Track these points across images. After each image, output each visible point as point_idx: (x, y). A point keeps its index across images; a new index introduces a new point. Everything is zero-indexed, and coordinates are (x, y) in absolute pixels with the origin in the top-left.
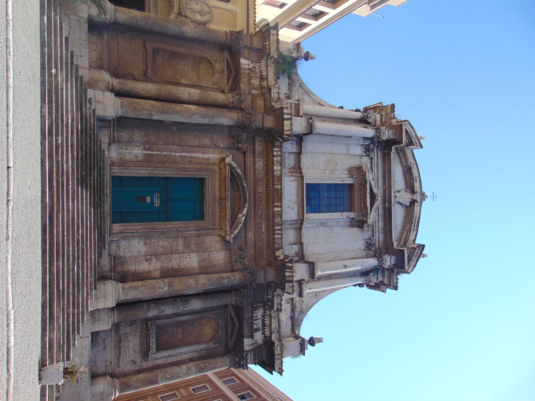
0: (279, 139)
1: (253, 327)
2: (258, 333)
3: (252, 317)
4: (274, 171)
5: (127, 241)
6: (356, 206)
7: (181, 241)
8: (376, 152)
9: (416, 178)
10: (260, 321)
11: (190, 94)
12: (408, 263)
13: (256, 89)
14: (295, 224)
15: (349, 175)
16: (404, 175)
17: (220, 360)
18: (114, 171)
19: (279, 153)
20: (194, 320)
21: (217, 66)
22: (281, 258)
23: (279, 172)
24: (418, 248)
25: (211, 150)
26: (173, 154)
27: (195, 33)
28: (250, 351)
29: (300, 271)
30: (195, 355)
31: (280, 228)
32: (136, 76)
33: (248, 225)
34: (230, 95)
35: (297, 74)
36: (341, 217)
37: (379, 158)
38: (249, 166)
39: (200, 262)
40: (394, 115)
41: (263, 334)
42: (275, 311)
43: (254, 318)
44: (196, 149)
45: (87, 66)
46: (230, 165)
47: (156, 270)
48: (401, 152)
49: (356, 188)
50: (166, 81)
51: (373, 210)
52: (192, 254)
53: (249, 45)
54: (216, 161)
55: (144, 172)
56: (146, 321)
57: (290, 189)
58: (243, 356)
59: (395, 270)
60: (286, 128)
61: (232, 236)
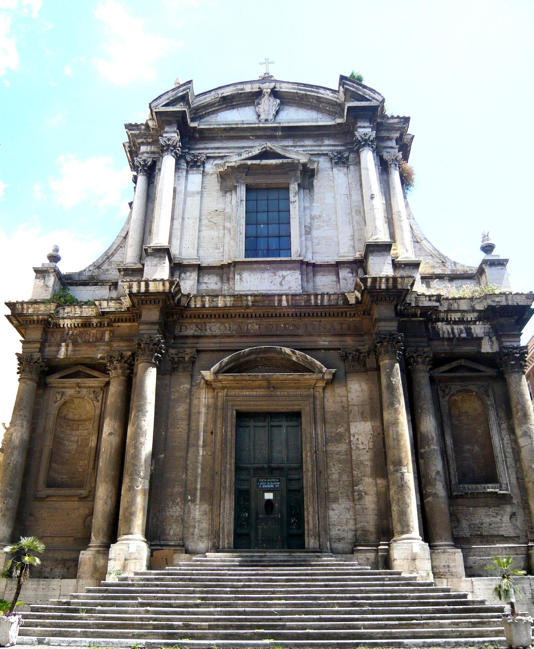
0: (176, 299)
1: (464, 338)
2: (473, 331)
3: (449, 340)
4: (226, 307)
5: (331, 527)
6: (280, 180)
7: (332, 448)
8: (198, 152)
9: (238, 89)
10: (455, 327)
11: (110, 434)
12: (368, 100)
13: (103, 334)
14: (307, 275)
15: (233, 192)
16: (233, 107)
17: (513, 388)
18: (226, 545)
19: (199, 299)
20: (453, 427)
21: (70, 392)
22: (359, 295)
23: (228, 299)
24: (345, 86)
25: (195, 402)
26: (200, 458)
27: (22, 426)
28: (500, 343)
29: (381, 268)
30: (504, 426)
31: (312, 297)
32: (87, 512)
33: (309, 345)
34: (113, 373)
35: (80, 273)
36: (297, 204)
37: (207, 146)
38: (218, 345)
39: (364, 418)
40: (142, 124)
41: (474, 323)
42: (441, 305)
43: (451, 336)
44: (193, 424)
45: (74, 581)
46: (216, 373)
47: (376, 485)
48: (200, 113)
49: (251, 180)
50: (94, 469)
51: (287, 155)
52: (352, 431)
53: (38, 345)
54: (211, 395)
55: (227, 502)
56: (451, 497)
57: (253, 283)
58: (507, 354)
59: (379, 120)
60: (161, 288)
61: (324, 369)
